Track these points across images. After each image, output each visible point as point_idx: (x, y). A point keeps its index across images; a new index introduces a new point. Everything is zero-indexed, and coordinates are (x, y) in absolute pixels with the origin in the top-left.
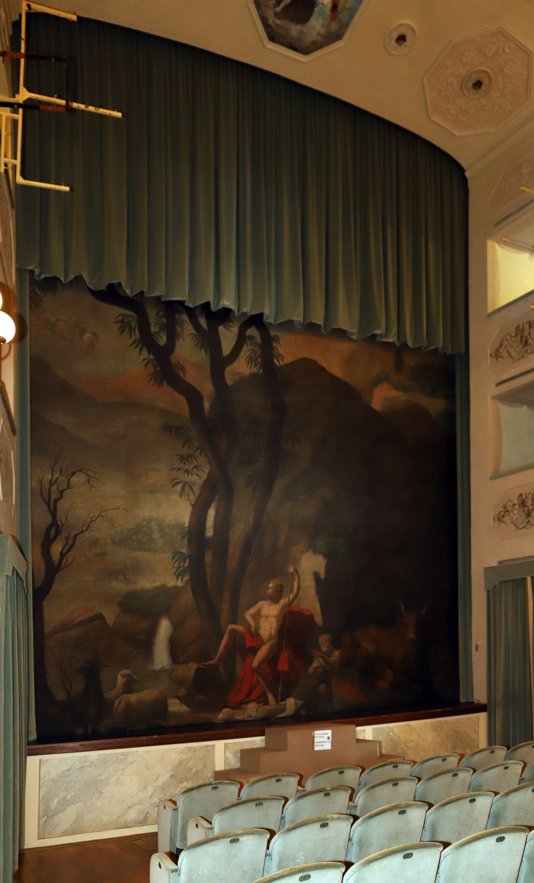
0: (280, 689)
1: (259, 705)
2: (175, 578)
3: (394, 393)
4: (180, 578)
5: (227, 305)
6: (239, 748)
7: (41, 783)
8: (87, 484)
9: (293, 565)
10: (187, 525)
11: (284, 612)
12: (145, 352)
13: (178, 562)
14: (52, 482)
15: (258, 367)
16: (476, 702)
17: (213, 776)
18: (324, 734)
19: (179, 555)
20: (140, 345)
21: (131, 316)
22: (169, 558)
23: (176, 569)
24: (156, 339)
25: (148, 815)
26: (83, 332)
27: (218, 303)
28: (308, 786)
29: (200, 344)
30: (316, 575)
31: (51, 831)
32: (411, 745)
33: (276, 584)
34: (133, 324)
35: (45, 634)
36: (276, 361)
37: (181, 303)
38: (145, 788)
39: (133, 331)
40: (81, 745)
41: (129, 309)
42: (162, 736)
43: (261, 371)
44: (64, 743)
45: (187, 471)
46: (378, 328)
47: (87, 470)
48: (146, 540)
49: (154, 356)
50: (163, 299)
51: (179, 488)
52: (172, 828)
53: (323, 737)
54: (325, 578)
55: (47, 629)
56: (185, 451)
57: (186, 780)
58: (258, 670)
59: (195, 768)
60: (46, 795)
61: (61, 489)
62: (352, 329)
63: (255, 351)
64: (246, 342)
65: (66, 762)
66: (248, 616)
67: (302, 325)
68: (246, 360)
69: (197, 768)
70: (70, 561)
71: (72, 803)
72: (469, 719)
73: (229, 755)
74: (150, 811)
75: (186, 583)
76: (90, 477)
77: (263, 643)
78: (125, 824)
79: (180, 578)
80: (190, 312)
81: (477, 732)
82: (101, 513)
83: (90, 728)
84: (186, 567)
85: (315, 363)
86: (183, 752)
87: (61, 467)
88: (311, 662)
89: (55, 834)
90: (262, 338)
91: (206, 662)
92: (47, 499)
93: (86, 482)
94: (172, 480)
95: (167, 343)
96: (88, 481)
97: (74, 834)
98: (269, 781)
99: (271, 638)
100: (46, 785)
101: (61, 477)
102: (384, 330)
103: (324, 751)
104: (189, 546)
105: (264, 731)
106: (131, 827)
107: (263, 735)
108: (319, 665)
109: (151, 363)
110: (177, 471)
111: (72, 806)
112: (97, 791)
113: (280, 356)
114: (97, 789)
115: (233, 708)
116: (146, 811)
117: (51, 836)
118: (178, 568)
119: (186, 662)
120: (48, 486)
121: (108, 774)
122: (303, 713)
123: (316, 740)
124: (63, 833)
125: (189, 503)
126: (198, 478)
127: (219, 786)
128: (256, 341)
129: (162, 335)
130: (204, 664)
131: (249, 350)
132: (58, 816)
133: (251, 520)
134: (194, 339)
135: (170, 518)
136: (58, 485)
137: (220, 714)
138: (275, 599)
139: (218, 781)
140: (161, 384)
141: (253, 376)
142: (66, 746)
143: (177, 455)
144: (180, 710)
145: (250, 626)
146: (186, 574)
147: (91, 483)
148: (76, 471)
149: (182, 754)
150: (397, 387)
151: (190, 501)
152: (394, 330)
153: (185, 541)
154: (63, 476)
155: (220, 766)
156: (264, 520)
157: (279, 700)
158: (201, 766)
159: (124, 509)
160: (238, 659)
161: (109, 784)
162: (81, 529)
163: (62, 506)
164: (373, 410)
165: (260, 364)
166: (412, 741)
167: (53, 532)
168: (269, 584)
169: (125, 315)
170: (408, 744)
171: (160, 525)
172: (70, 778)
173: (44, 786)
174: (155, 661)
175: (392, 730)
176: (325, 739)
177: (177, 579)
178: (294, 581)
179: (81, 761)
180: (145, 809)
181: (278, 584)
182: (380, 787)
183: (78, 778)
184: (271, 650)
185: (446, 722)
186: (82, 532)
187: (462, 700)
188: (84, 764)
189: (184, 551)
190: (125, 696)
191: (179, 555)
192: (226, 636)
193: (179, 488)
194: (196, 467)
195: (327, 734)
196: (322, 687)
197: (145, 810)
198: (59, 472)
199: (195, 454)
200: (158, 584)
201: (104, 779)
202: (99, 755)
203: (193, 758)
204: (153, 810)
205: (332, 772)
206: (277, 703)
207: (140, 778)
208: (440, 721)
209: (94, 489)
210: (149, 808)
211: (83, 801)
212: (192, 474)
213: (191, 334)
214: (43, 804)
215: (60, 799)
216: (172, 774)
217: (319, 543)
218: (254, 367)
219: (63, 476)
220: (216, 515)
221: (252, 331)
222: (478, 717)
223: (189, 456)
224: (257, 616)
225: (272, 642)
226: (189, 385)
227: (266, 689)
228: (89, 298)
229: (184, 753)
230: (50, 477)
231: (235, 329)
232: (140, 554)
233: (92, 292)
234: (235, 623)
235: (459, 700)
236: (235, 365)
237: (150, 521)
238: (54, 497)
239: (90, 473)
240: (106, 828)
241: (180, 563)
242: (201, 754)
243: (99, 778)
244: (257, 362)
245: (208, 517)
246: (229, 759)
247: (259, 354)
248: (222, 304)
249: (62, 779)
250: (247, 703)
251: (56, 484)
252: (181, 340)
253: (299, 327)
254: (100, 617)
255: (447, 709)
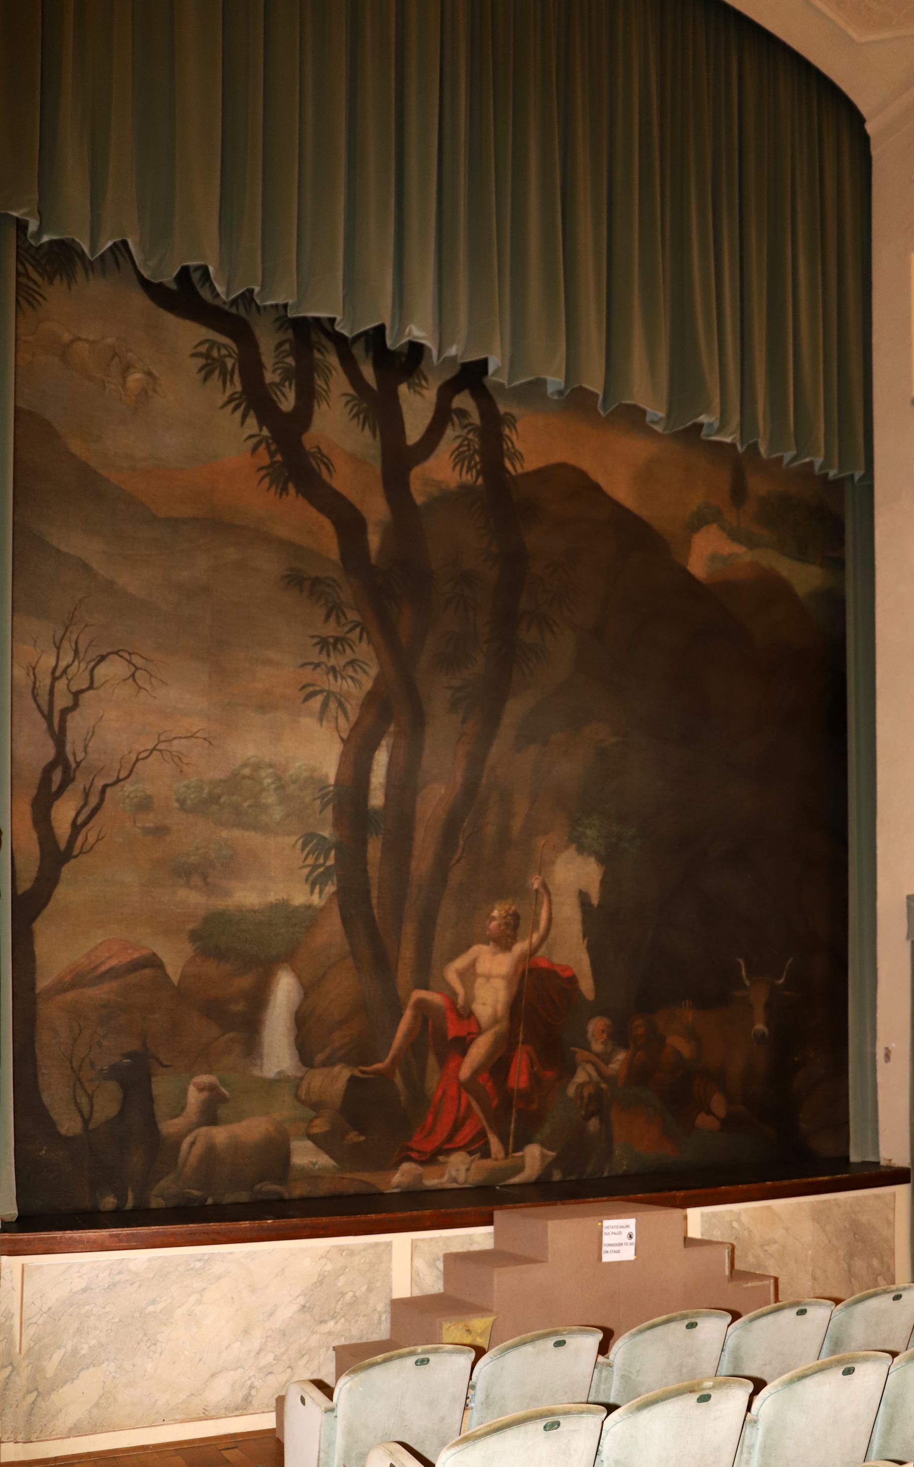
0: (512, 1126)
1: (473, 1157)
2: (307, 888)
3: (730, 548)
4: (317, 890)
5: (418, 338)
6: (440, 1252)
7: (23, 1317)
8: (130, 681)
9: (540, 874)
10: (332, 780)
11: (520, 969)
12: (252, 422)
13: (313, 855)
14: (57, 674)
15: (474, 471)
16: (883, 1163)
17: (389, 1309)
18: (622, 1227)
19: (315, 841)
20: (243, 407)
21: (225, 346)
22: (294, 846)
23: (309, 869)
24: (275, 398)
25: (253, 1392)
26: (127, 368)
27: (400, 332)
28: (617, 1355)
29: (361, 416)
30: (583, 898)
31: (45, 1425)
32: (773, 1248)
33: (506, 912)
34: (230, 363)
35: (37, 991)
36: (508, 465)
37: (325, 327)
38: (246, 1332)
39: (228, 377)
40: (111, 1236)
41: (221, 331)
42: (283, 1222)
43: (480, 481)
44: (75, 1232)
45: (333, 669)
46: (707, 410)
47: (130, 654)
48: (250, 806)
49: (270, 430)
50: (291, 314)
51: (316, 703)
52: (322, 1455)
53: (620, 1233)
54: (599, 905)
55: (43, 983)
56: (331, 630)
57: (333, 1317)
58: (469, 1086)
59: (351, 1291)
60: (35, 1344)
61: (74, 688)
62: (656, 412)
63: (469, 440)
64: (452, 421)
65: (79, 1272)
66: (452, 973)
67: (560, 393)
68: (451, 455)
69: (354, 1292)
70: (92, 839)
71: (91, 1364)
72: (877, 1197)
73: (420, 1263)
74: (257, 1383)
75: (330, 900)
76: (137, 668)
77: (480, 1031)
78: (204, 1411)
79: (317, 890)
80: (342, 344)
81: (891, 1224)
82: (156, 745)
83: (130, 1195)
84: (330, 866)
85: (582, 475)
86: (326, 1256)
87: (76, 643)
88: (572, 1072)
89: (54, 1432)
90: (482, 416)
91: (368, 1065)
92: (45, 708)
93: (128, 678)
94: (304, 687)
95: (296, 408)
96: (133, 676)
97: (95, 1433)
98: (540, 1344)
99: (495, 1021)
100: (36, 1323)
101: (76, 663)
102: (718, 416)
103: (619, 1263)
104: (337, 824)
105: (492, 1215)
106: (217, 1419)
107: (490, 1222)
108: (587, 1079)
109: (263, 445)
110: (314, 669)
111: (92, 1369)
112: (145, 1339)
113: (517, 456)
114: (145, 1335)
115: (421, 1163)
116: (249, 1382)
117: (45, 1437)
118: (314, 867)
119: (328, 1063)
120: (48, 681)
121: (169, 1301)
122: (557, 1176)
123: (606, 1239)
124: (71, 1429)
125: (336, 735)
126: (355, 685)
127: (432, 1357)
128: (471, 421)
129: (286, 390)
130: (363, 1068)
131: (458, 437)
132: (60, 1391)
133: (459, 778)
134: (350, 405)
135: (297, 764)
136: (69, 681)
137: (396, 1173)
138: (504, 942)
139: (430, 1346)
140: (284, 490)
141: (465, 490)
142: (80, 1236)
143: (313, 637)
144: (314, 1164)
145: (455, 994)
146: (330, 882)
147: (137, 681)
148: (108, 654)
149: (324, 1261)
150: (735, 536)
151: (338, 732)
152: (735, 419)
153: (329, 813)
154: (80, 663)
155: (402, 1289)
156: (484, 781)
157: (510, 1150)
158: (364, 1288)
159: (205, 739)
160: (432, 1060)
161: (172, 1323)
162: (115, 775)
163: (76, 725)
164: (691, 577)
165: (479, 467)
166: (775, 1242)
167: (57, 777)
168: (492, 910)
169: (213, 344)
170: (766, 1248)
171: (278, 778)
172: (87, 1308)
173: (32, 1323)
174: (265, 1060)
175: (738, 1216)
176: (624, 1238)
177: (312, 892)
178: (541, 909)
179: (111, 1270)
180: (247, 1378)
181: (511, 912)
182: (818, 1378)
183: (104, 1308)
184: (497, 1043)
185: (837, 1203)
186: (118, 780)
187: (854, 1158)
188: (117, 1278)
189: (327, 832)
190: (203, 1130)
191: (315, 841)
192: (408, 1014)
193: (316, 703)
194: (352, 662)
195: (627, 1226)
196: (594, 1124)
197: (246, 1381)
198: (72, 654)
199: (349, 636)
200: (272, 898)
201: (161, 1312)
202: (149, 1260)
203: (347, 1270)
204: (263, 1381)
205: (672, 1325)
206: (507, 1154)
207: (237, 1311)
208: (825, 1201)
209: (143, 692)
210: (254, 1376)
211: (115, 1359)
212: (343, 678)
213: (346, 395)
214: (30, 1363)
215: (65, 1353)
216: (303, 1303)
217: (588, 832)
218: (467, 472)
219: (80, 663)
220: (391, 764)
221: (463, 401)
222: (894, 1194)
223: (337, 640)
224: (469, 975)
225: (497, 1028)
226: (338, 496)
227: (485, 1123)
228: (140, 300)
229: (329, 1259)
230: (53, 662)
231: (431, 394)
232: (237, 833)
233: (145, 284)
234: (426, 988)
235: (848, 1158)
236: (431, 464)
237: (257, 767)
238: (61, 702)
239: (136, 659)
240: (164, 1420)
241: (317, 859)
242: (362, 1261)
243: (151, 1308)
244: (473, 463)
245: (375, 767)
246: (421, 1274)
247: (477, 447)
248: (410, 333)
249: (72, 1309)
250: (448, 1152)
251: (64, 677)
252: (324, 406)
253: (556, 397)
254: (153, 962)
255: (839, 1176)
